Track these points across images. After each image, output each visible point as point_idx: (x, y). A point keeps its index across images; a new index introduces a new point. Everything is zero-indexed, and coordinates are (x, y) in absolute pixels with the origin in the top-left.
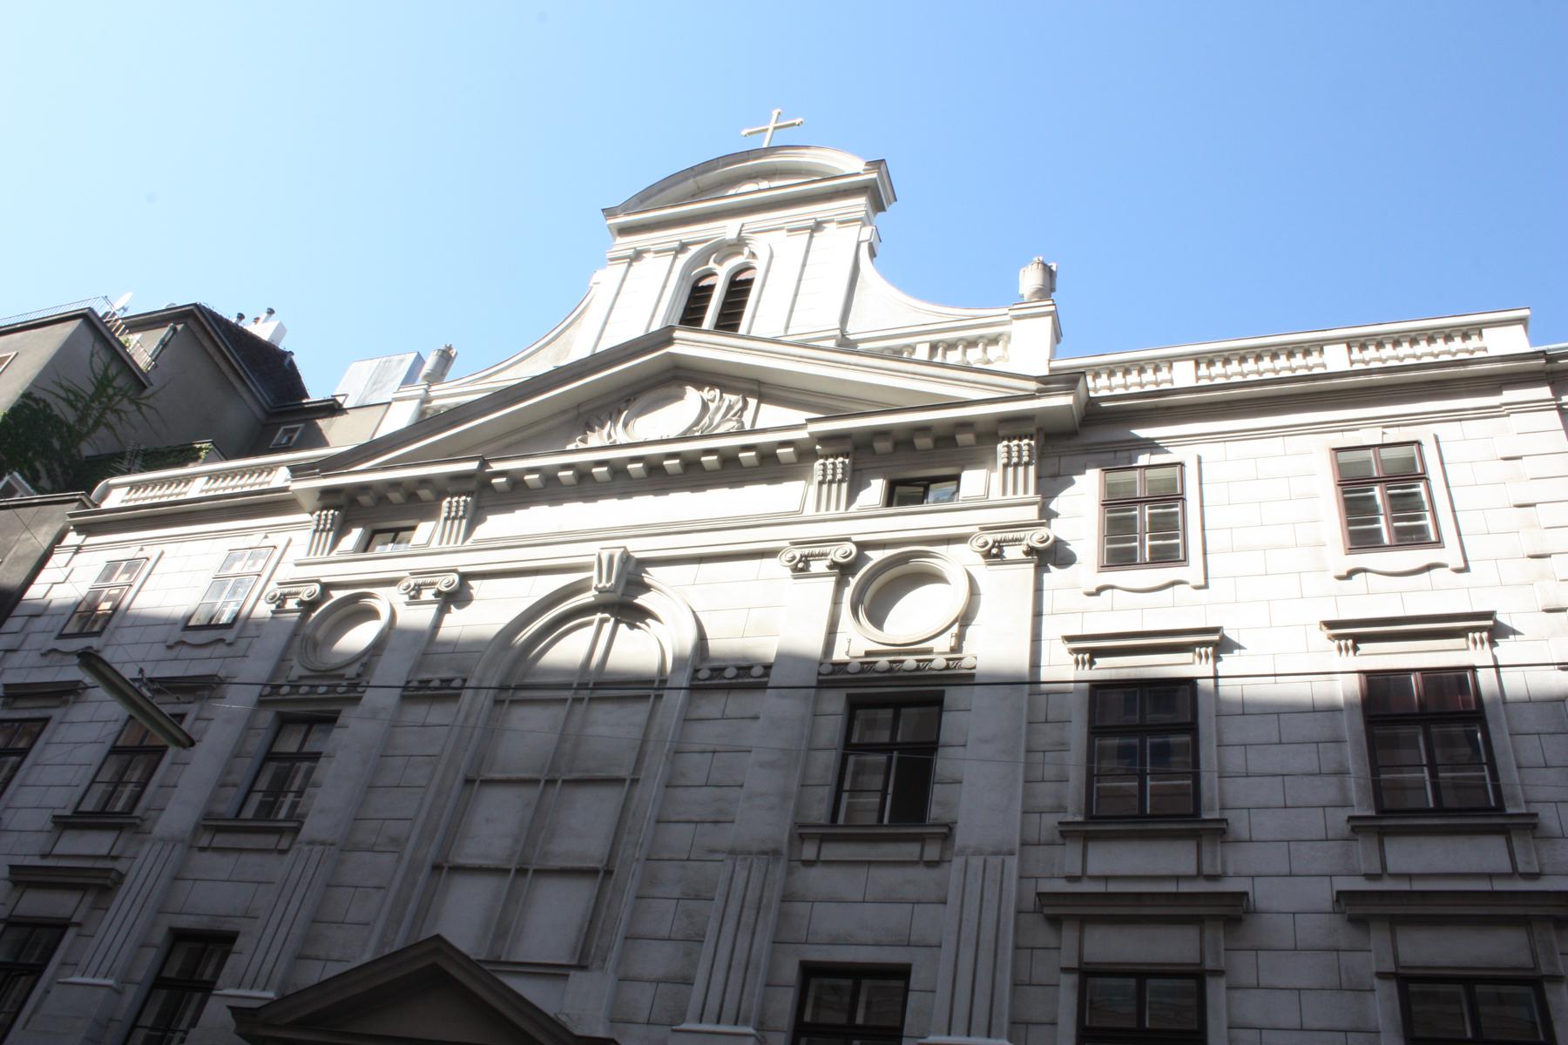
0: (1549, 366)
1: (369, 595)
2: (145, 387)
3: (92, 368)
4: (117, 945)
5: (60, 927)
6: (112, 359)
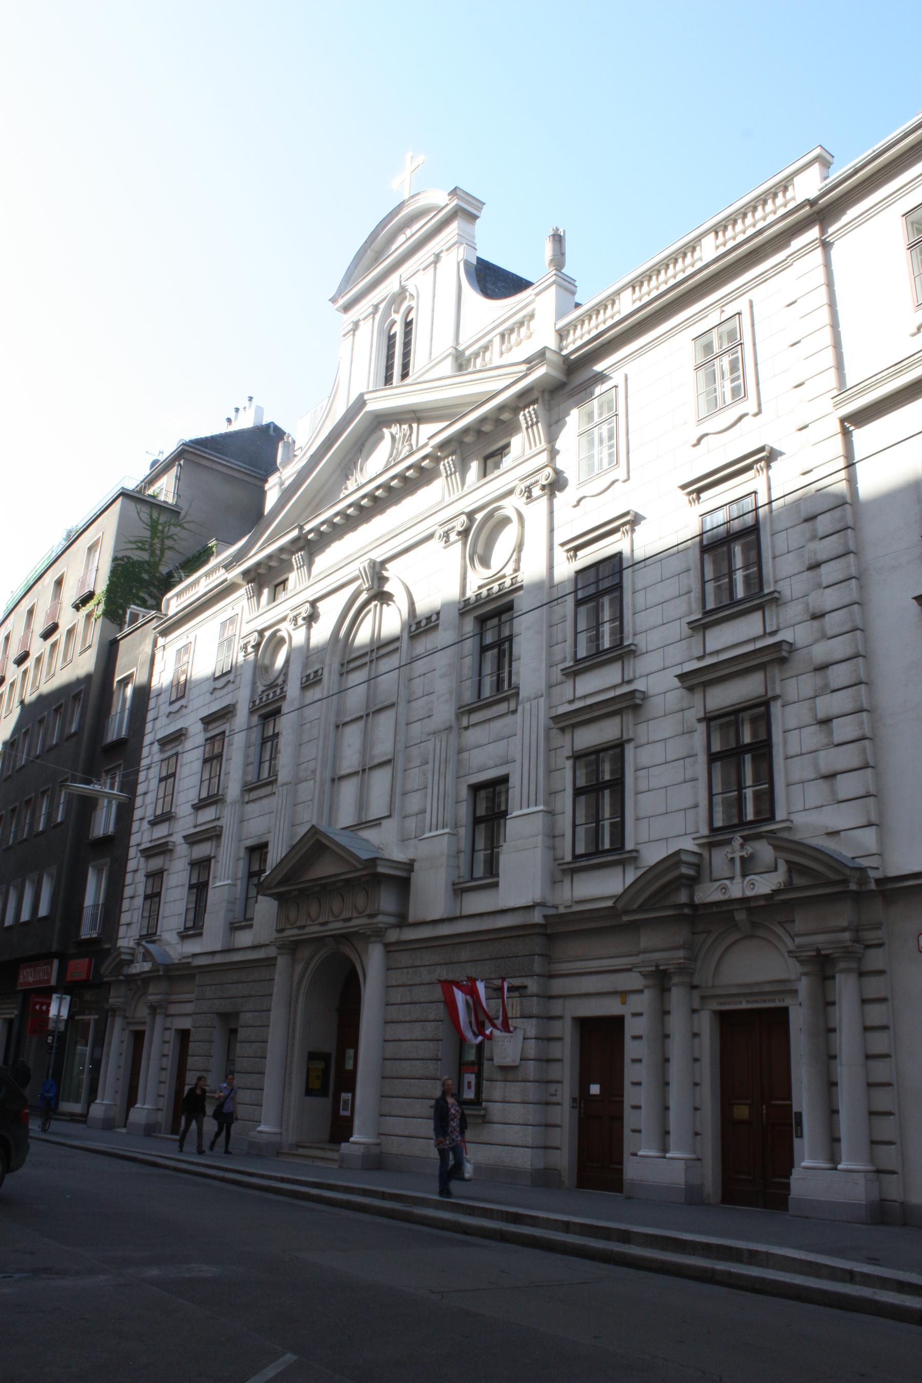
0: (815, 208)
1: (499, 508)
2: (179, 513)
3: (144, 522)
4: (228, 863)
5: (617, 748)
6: (151, 508)
